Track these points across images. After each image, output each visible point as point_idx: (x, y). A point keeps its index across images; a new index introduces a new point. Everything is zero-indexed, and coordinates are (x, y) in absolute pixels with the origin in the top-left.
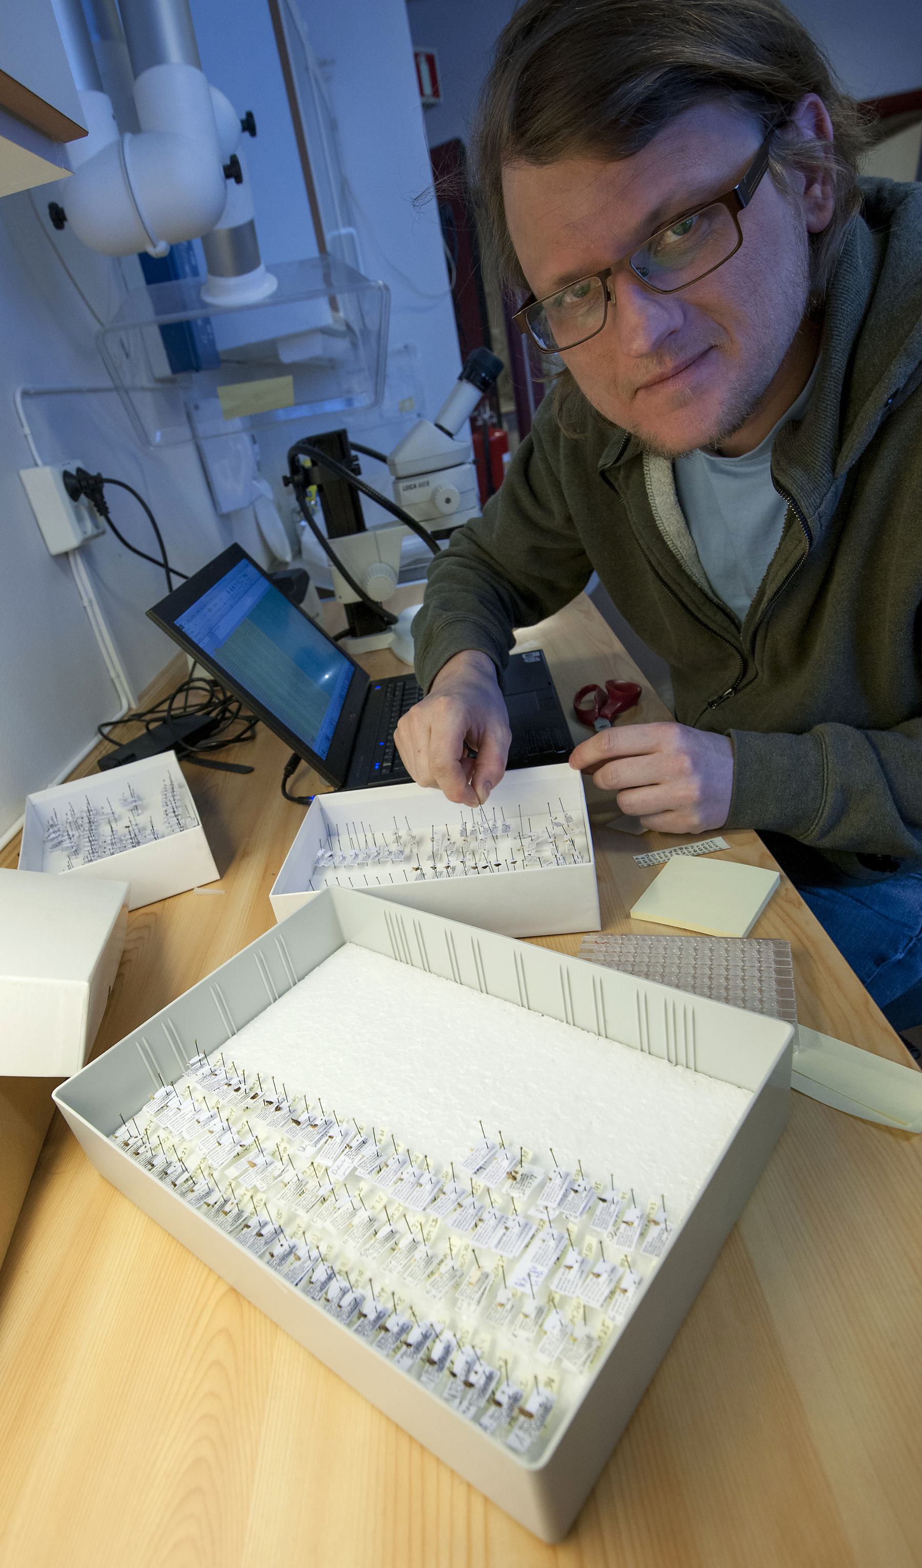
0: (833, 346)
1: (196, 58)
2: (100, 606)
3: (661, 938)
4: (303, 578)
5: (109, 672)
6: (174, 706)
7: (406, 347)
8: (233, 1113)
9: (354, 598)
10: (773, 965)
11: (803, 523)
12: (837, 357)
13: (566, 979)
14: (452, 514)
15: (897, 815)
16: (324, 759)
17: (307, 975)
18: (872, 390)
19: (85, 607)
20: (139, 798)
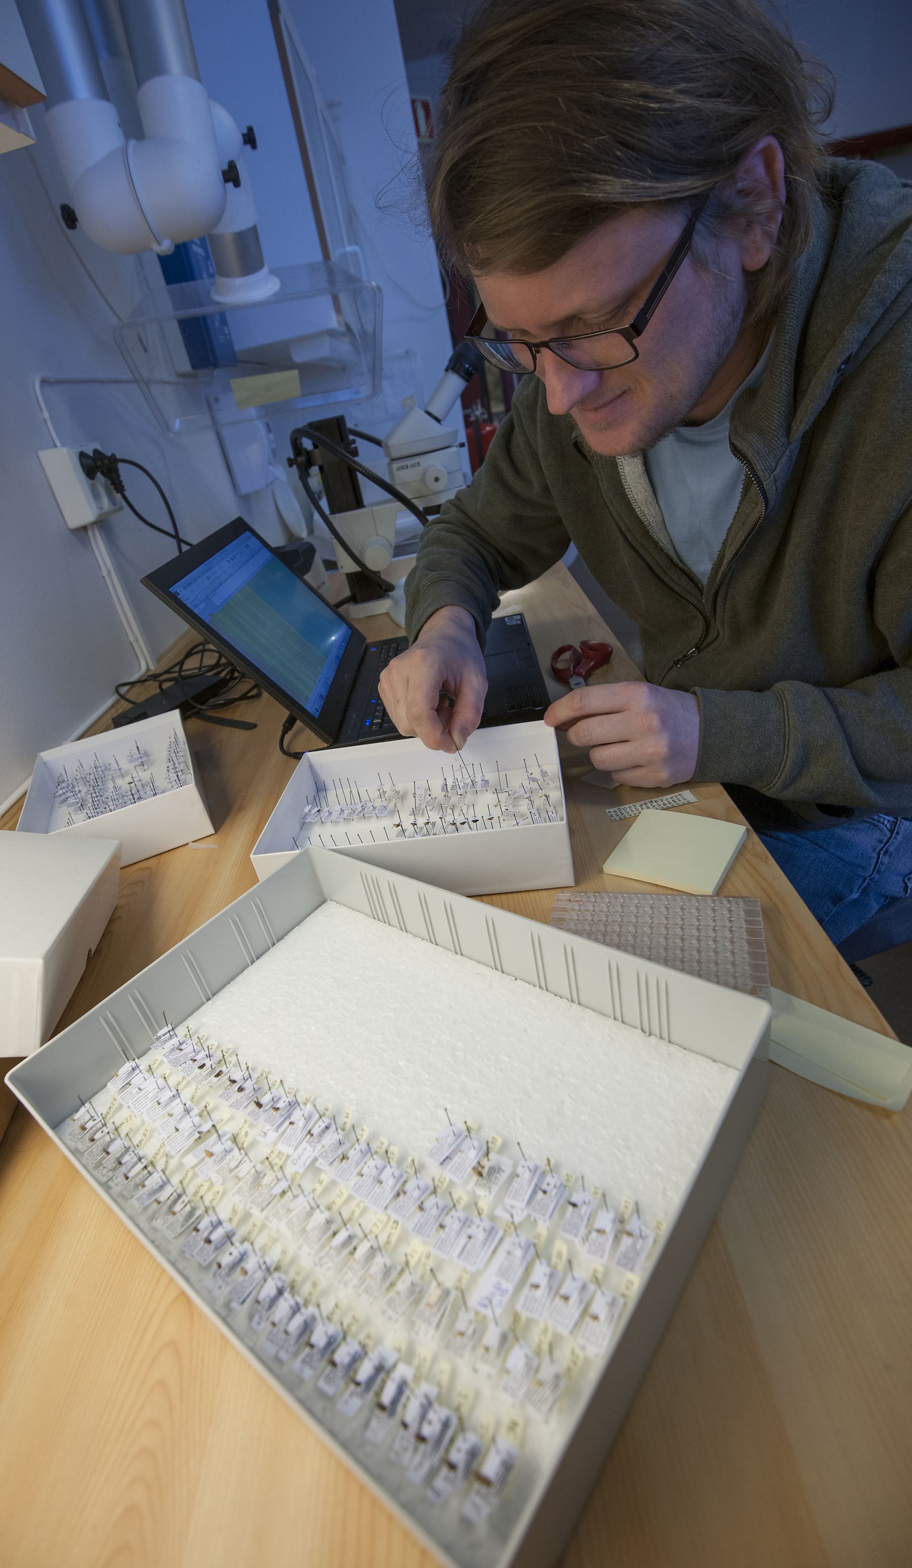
0: (787, 313)
1: (195, 71)
2: (117, 576)
3: (633, 896)
4: (310, 551)
5: (128, 636)
6: (184, 668)
7: (407, 352)
8: (198, 1090)
9: (352, 567)
10: (744, 926)
11: (759, 486)
12: (791, 324)
13: (537, 946)
14: (440, 492)
15: (855, 769)
16: (317, 717)
17: (286, 934)
18: (824, 357)
19: (104, 577)
20: (146, 754)
